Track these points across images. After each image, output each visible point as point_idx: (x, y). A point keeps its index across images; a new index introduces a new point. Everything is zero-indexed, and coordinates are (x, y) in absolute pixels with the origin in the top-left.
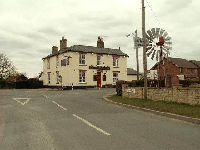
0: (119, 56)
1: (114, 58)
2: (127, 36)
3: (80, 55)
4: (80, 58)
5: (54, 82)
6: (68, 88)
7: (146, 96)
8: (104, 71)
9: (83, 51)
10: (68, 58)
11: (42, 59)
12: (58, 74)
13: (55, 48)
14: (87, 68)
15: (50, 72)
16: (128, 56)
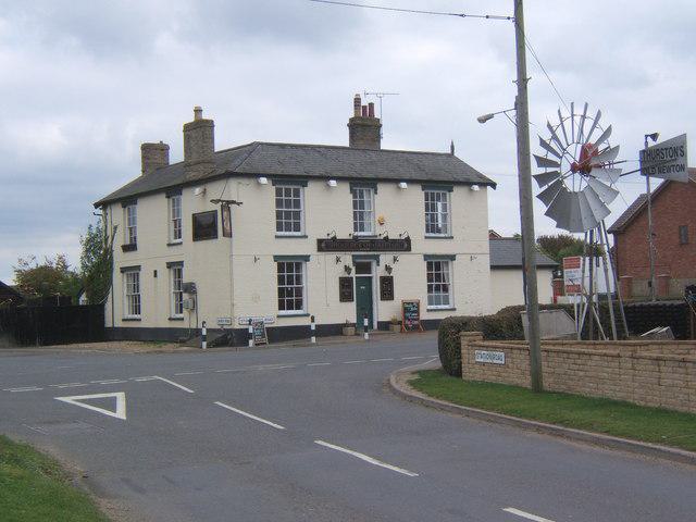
0: (449, 185)
1: (426, 195)
2: (483, 120)
3: (278, 193)
4: (279, 203)
5: (158, 311)
6: (231, 338)
7: (537, 376)
8: (386, 258)
9: (288, 172)
10: (227, 205)
11: (96, 205)
12: (179, 274)
13: (153, 153)
14: (307, 247)
15: (138, 268)
16: (494, 185)
